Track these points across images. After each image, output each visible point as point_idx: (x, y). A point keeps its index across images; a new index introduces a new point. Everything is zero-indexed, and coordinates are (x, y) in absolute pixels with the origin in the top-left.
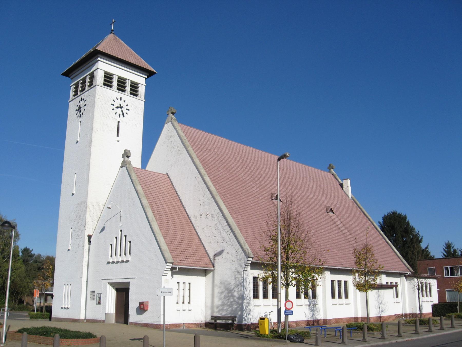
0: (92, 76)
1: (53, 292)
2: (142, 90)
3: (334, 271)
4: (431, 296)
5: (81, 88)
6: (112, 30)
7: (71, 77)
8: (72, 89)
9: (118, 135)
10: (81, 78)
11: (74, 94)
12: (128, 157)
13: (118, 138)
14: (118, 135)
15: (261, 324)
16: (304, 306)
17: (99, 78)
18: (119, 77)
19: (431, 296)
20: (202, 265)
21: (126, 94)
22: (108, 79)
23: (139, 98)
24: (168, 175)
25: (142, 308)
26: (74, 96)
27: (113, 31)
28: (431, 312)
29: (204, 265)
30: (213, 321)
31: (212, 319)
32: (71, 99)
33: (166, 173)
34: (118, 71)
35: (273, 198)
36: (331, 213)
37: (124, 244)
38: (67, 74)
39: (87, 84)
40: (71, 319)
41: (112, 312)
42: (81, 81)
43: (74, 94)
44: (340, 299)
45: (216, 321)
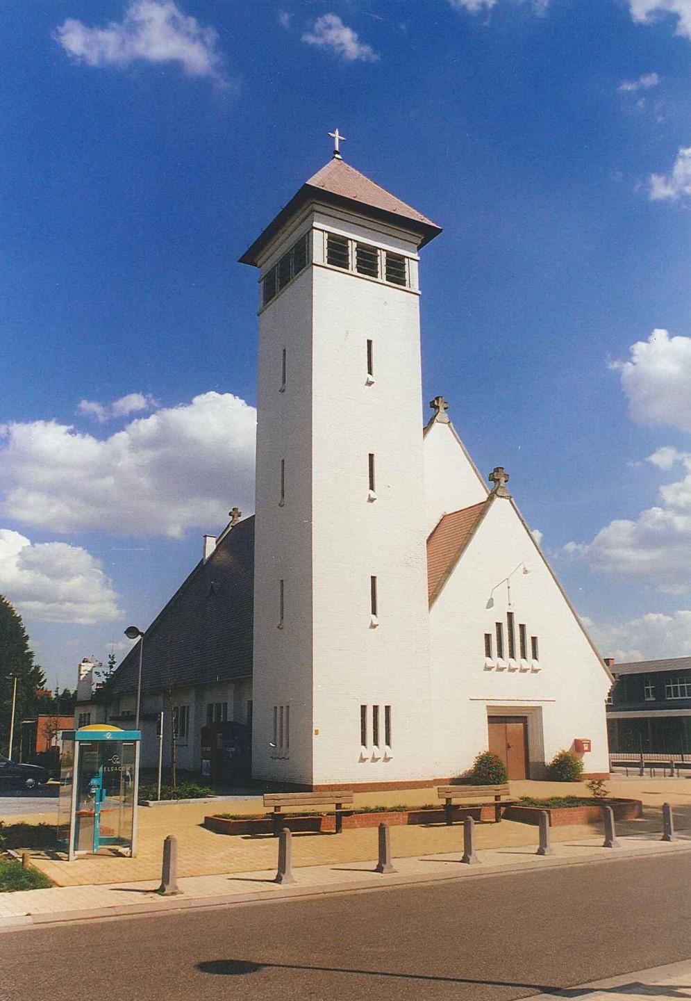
2: (412, 271)
23: (406, 288)
34: (355, 237)
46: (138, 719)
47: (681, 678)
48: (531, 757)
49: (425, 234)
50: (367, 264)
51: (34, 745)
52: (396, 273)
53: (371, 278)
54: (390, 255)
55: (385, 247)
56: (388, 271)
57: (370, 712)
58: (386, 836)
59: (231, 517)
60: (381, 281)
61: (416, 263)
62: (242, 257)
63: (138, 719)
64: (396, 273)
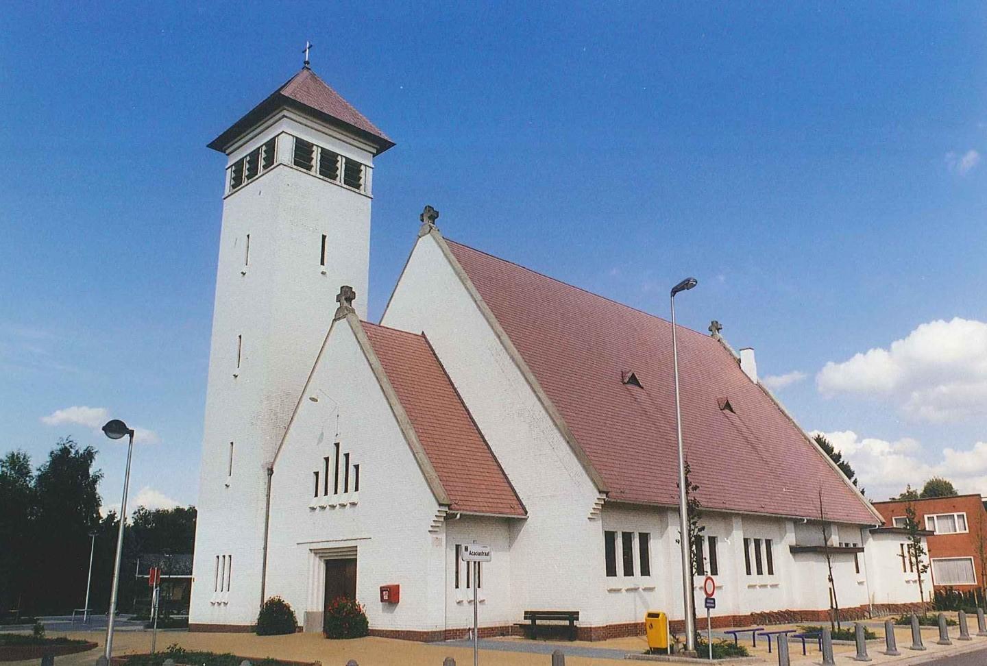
0: (271, 146)
1: (191, 574)
2: (367, 176)
3: (748, 518)
4: (771, 572)
5: (246, 172)
6: (305, 62)
7: (227, 152)
8: (229, 174)
9: (322, 263)
10: (249, 152)
11: (233, 182)
12: (349, 300)
13: (323, 268)
14: (322, 263)
15: (651, 626)
16: (624, 589)
17: (285, 150)
18: (309, 168)
19: (771, 572)
20: (503, 510)
21: (338, 183)
22: (302, 153)
23: (362, 192)
24: (425, 337)
25: (390, 596)
26: (234, 187)
27: (308, 63)
28: (321, 608)
29: (508, 510)
30: (529, 622)
31: (525, 618)
32: (227, 192)
33: (420, 334)
34: (321, 140)
35: (626, 381)
36: (727, 411)
37: (339, 473)
38: (222, 144)
39: (262, 163)
40: (234, 626)
41: (320, 610)
42: (248, 158)
43: (233, 182)
44: (760, 576)
45: (534, 622)
46: (113, 607)
47: (18, 614)
48: (854, 563)
49: (381, 145)
50: (328, 166)
51: (42, 661)
52: (353, 176)
53: (331, 181)
54: (348, 161)
55: (346, 150)
56: (345, 180)
57: (225, 589)
58: (14, 662)
59: (339, 303)
60: (340, 184)
61: (371, 169)
62: (212, 143)
63: (113, 607)
64: (353, 176)
